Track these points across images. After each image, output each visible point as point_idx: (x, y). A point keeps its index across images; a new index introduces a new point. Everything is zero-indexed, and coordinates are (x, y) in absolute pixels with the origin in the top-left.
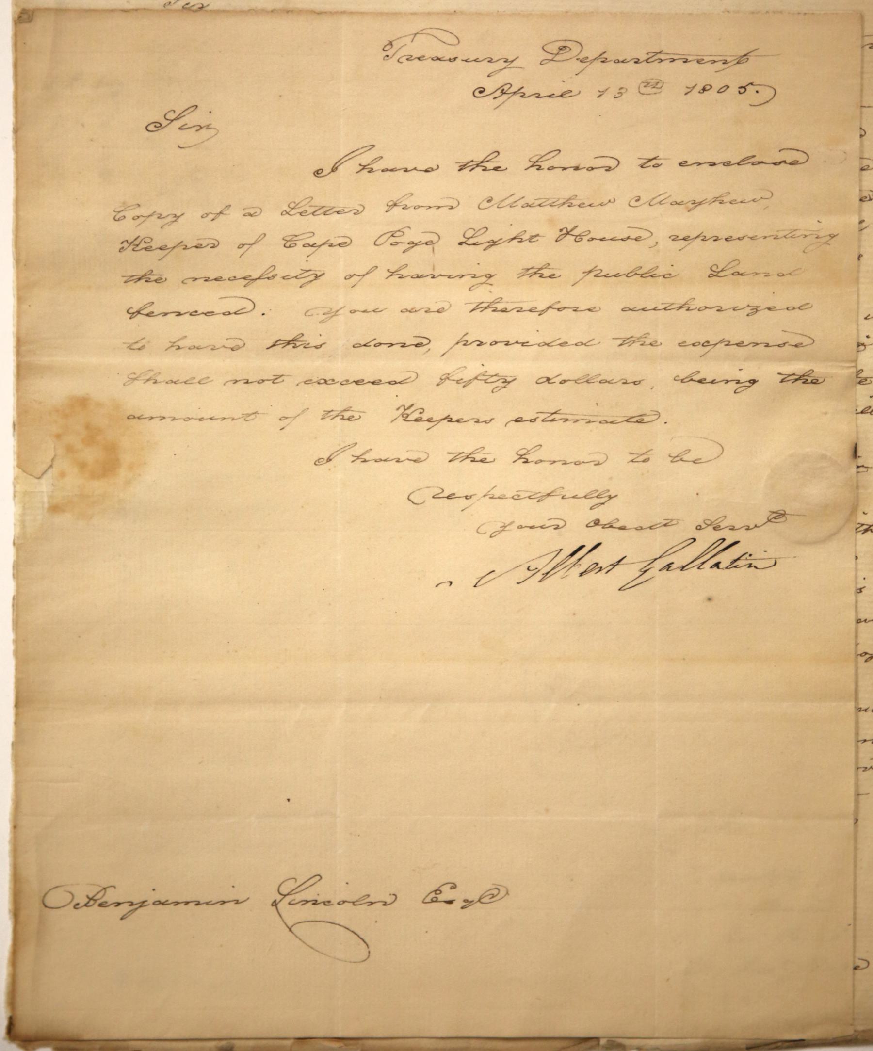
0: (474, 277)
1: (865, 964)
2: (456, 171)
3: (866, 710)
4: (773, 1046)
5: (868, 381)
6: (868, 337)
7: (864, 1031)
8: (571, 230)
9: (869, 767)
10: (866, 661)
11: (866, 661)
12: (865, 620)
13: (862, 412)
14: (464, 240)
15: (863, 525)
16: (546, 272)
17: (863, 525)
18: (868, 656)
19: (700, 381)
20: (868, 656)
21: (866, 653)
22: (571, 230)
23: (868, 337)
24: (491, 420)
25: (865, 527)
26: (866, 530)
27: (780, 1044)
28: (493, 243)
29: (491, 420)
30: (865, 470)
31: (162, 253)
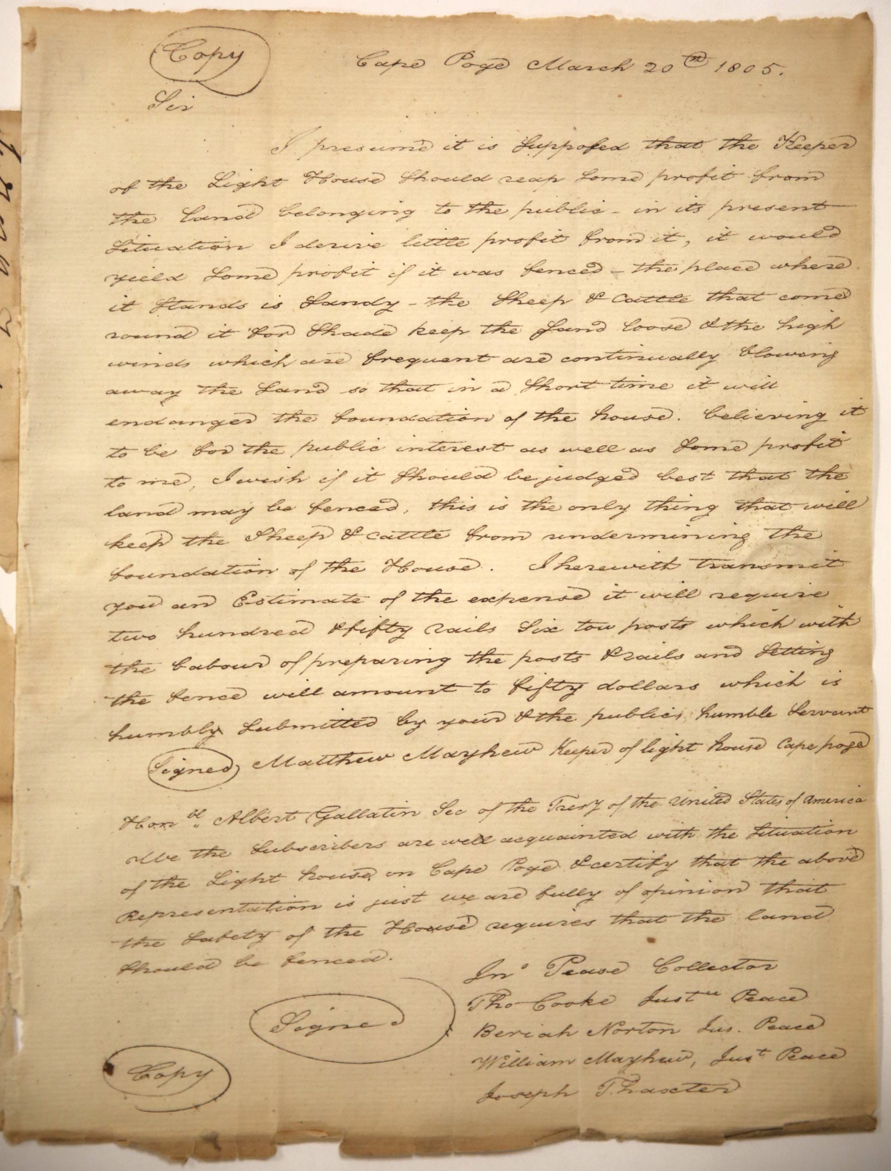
0: (430, 661)
1: (842, 1053)
2: (520, 510)
3: (842, 801)
4: (752, 1134)
5: (844, 476)
6: (843, 432)
7: (841, 1119)
8: (398, 561)
9: (845, 857)
10: (842, 753)
11: (842, 753)
12: (841, 713)
13: (838, 507)
14: (214, 181)
15: (838, 618)
16: (215, 540)
17: (838, 618)
18: (844, 748)
19: (525, 479)
20: (844, 748)
21: (842, 745)
22: (398, 561)
23: (843, 432)
24: (494, 146)
25: (841, 620)
26: (842, 624)
27: (757, 1132)
28: (316, 1028)
29: (494, 146)
30: (841, 564)
31: (299, 543)
